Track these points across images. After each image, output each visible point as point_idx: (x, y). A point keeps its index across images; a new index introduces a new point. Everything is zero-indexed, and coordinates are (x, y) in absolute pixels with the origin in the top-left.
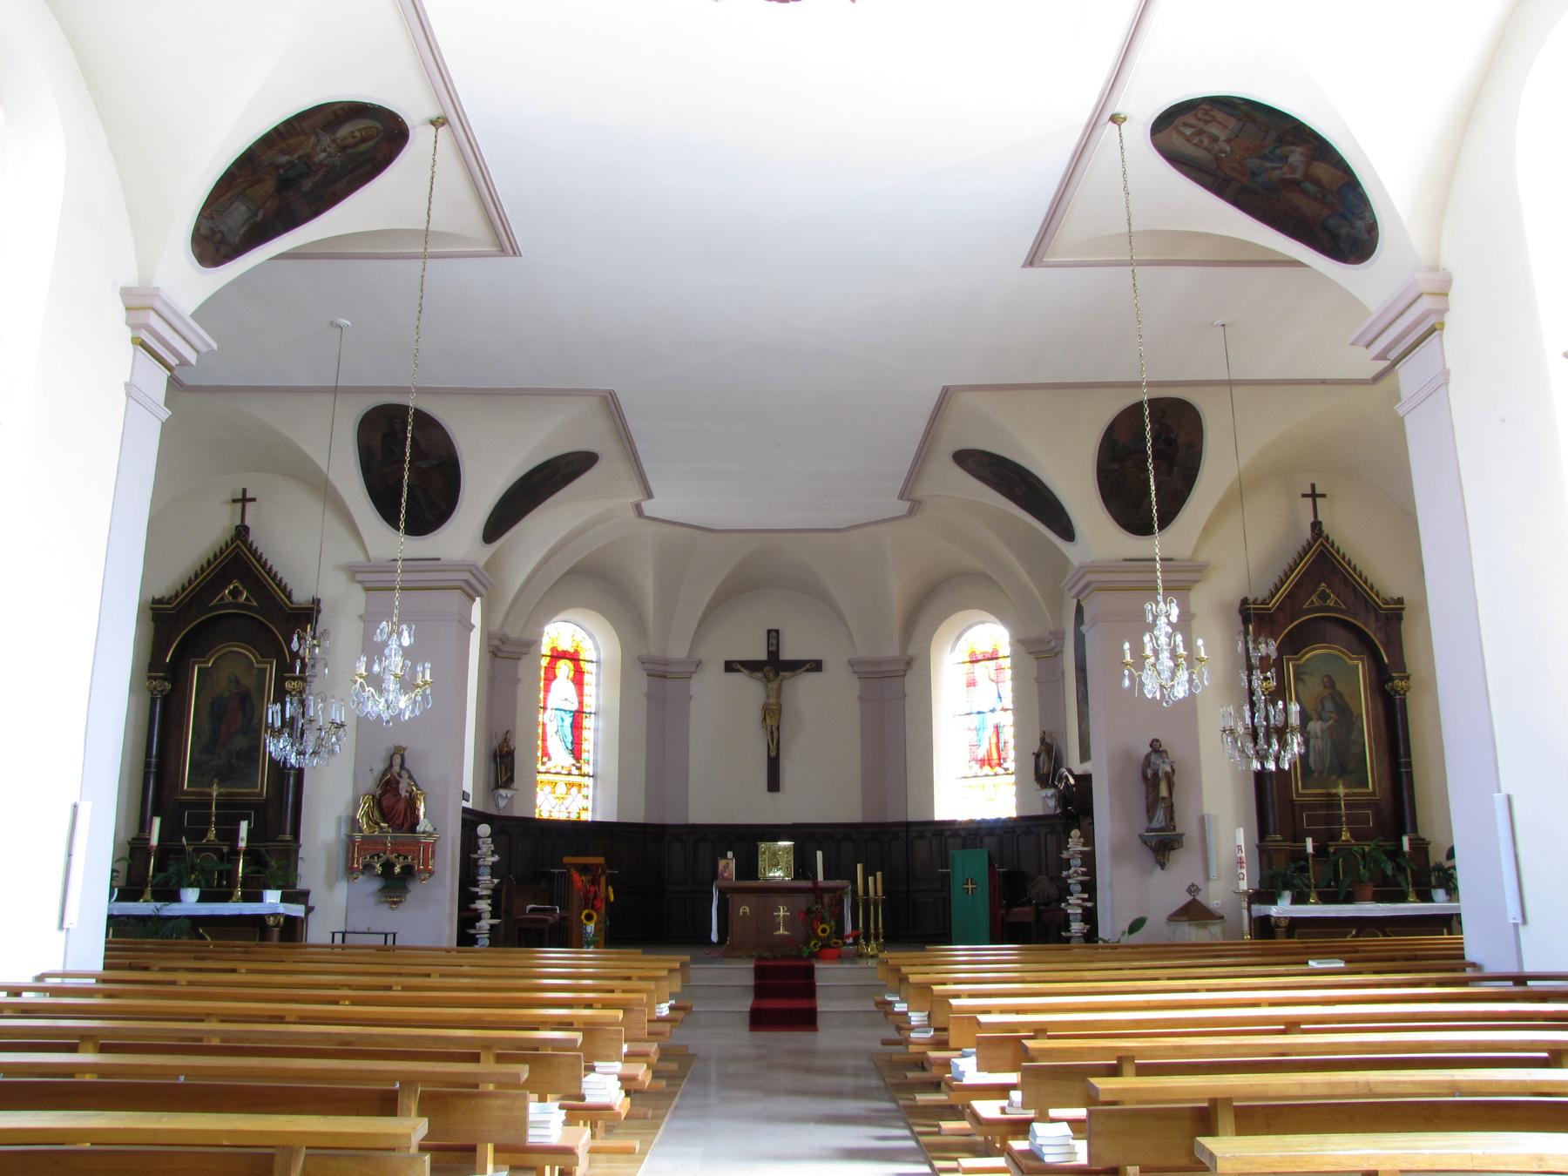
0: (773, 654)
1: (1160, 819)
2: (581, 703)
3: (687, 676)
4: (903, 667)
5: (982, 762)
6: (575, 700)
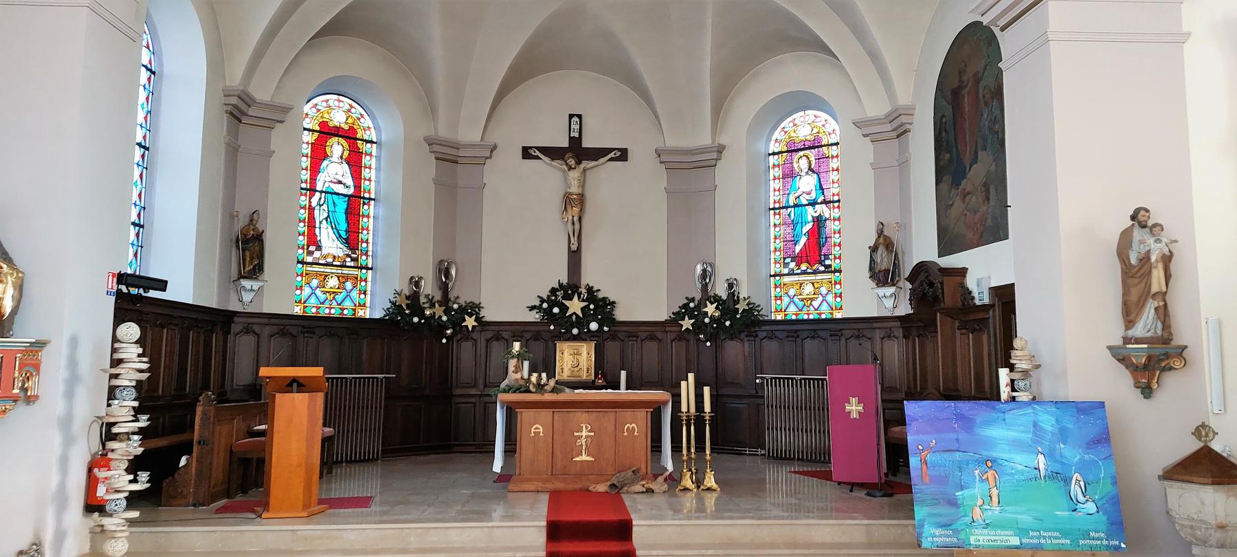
0: (575, 142)
1: (1146, 324)
2: (358, 187)
3: (480, 162)
4: (714, 155)
5: (799, 259)
6: (349, 181)
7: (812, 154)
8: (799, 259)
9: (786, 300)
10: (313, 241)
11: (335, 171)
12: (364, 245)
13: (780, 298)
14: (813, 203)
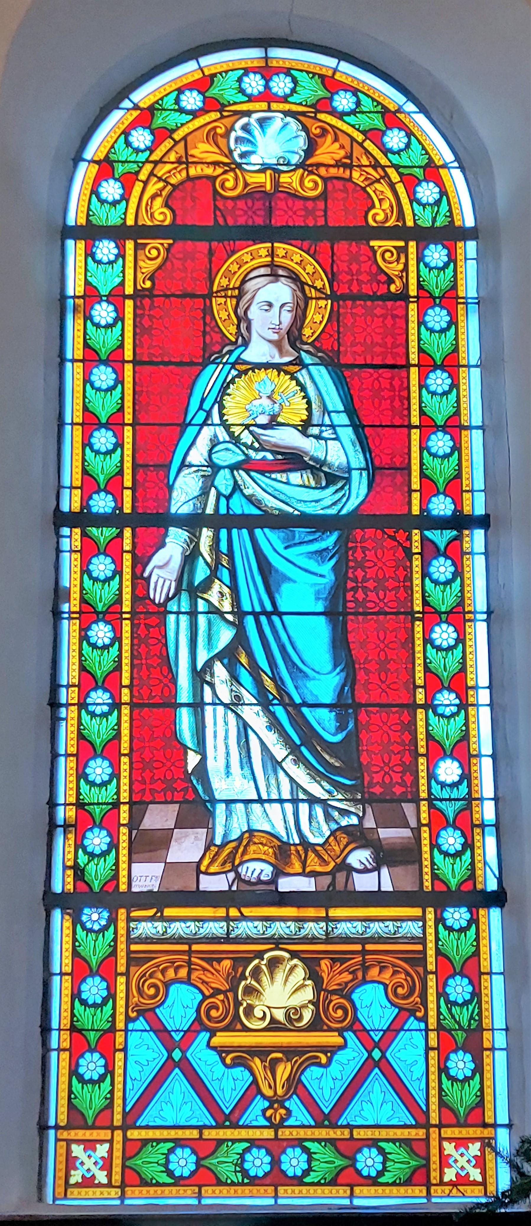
2: (386, 465)
6: (341, 450)
9: (143, 1052)
10: (166, 778)
11: (267, 398)
12: (449, 770)
13: (107, 1045)
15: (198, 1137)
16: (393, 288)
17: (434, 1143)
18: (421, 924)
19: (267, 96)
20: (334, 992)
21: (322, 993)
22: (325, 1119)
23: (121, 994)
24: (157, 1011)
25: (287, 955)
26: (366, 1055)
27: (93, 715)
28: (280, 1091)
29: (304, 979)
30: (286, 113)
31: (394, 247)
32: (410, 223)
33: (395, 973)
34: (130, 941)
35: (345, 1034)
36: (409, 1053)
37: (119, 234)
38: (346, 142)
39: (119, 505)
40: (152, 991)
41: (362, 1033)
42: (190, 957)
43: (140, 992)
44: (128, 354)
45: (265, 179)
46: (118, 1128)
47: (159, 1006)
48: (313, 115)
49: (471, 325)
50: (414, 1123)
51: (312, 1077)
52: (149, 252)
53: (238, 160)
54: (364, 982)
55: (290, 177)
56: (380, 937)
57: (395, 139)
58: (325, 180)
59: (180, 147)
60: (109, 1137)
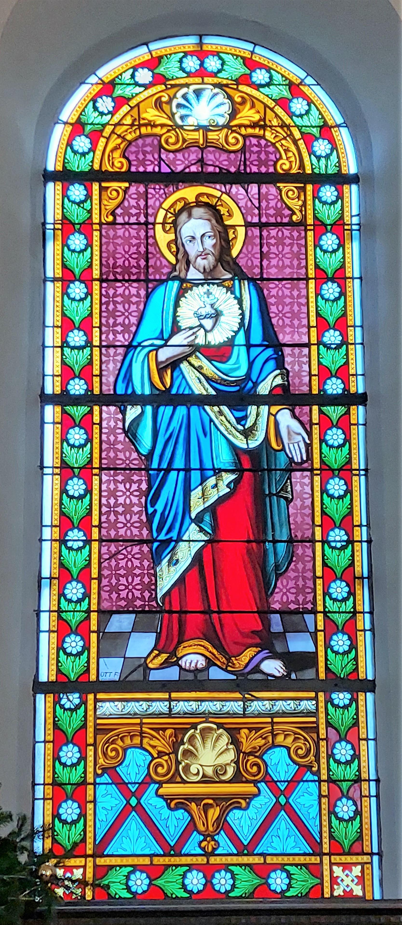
7: (235, 205)
8: (171, 620)
9: (108, 801)
13: (79, 792)
14: (238, 397)
15: (149, 863)
16: (294, 218)
17: (326, 867)
18: (314, 702)
19: (202, 73)
20: (250, 754)
21: (242, 754)
22: (243, 849)
23: (90, 758)
24: (118, 769)
25: (215, 726)
26: (275, 800)
27: (70, 549)
28: (211, 828)
29: (227, 744)
30: (215, 85)
31: (296, 187)
32: (309, 171)
33: (295, 739)
34: (96, 718)
35: (259, 785)
36: (306, 799)
37: (87, 178)
38: (260, 107)
39: (90, 388)
40: (114, 753)
41: (272, 783)
42: (141, 728)
43: (105, 754)
44: (96, 274)
45: (198, 136)
46: (90, 856)
47: (118, 766)
48: (235, 87)
49: (354, 248)
50: (311, 852)
51: (235, 817)
52: (111, 194)
53: (180, 122)
54: (274, 746)
55: (218, 135)
56: (284, 713)
57: (298, 106)
58: (245, 137)
59: (135, 112)
60: (83, 864)
